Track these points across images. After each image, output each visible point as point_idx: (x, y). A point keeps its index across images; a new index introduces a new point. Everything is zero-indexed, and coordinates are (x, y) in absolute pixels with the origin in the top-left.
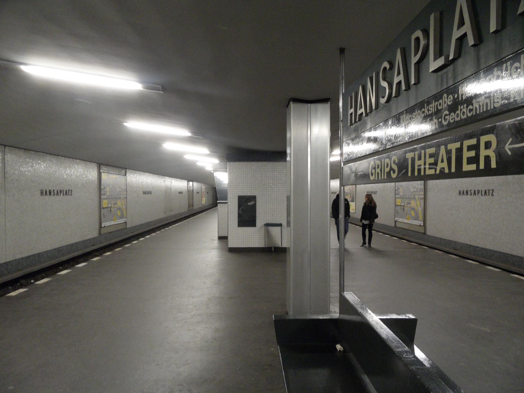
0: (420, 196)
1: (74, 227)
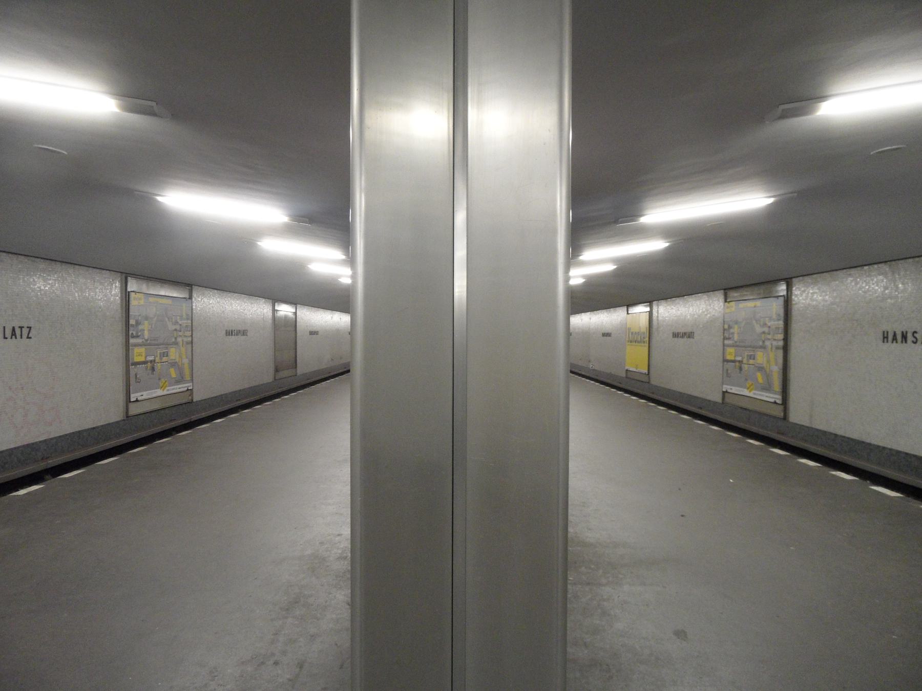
0: (775, 343)
1: (86, 401)
